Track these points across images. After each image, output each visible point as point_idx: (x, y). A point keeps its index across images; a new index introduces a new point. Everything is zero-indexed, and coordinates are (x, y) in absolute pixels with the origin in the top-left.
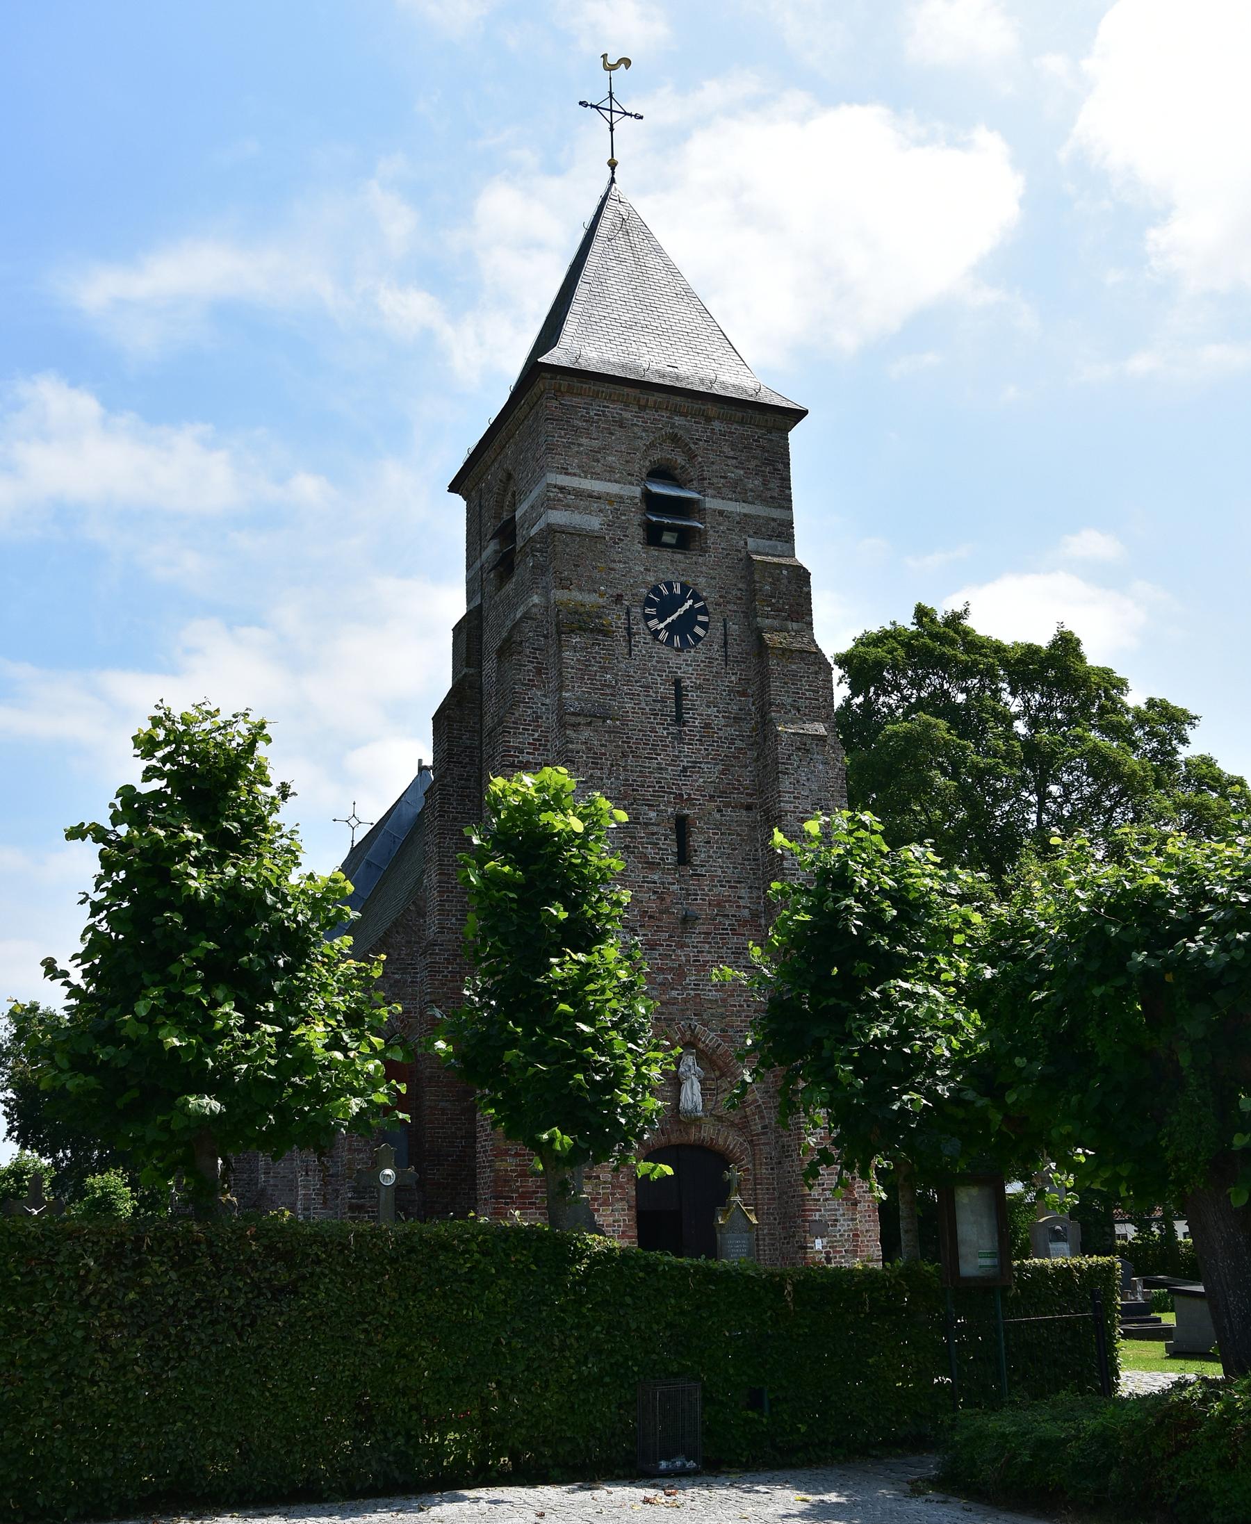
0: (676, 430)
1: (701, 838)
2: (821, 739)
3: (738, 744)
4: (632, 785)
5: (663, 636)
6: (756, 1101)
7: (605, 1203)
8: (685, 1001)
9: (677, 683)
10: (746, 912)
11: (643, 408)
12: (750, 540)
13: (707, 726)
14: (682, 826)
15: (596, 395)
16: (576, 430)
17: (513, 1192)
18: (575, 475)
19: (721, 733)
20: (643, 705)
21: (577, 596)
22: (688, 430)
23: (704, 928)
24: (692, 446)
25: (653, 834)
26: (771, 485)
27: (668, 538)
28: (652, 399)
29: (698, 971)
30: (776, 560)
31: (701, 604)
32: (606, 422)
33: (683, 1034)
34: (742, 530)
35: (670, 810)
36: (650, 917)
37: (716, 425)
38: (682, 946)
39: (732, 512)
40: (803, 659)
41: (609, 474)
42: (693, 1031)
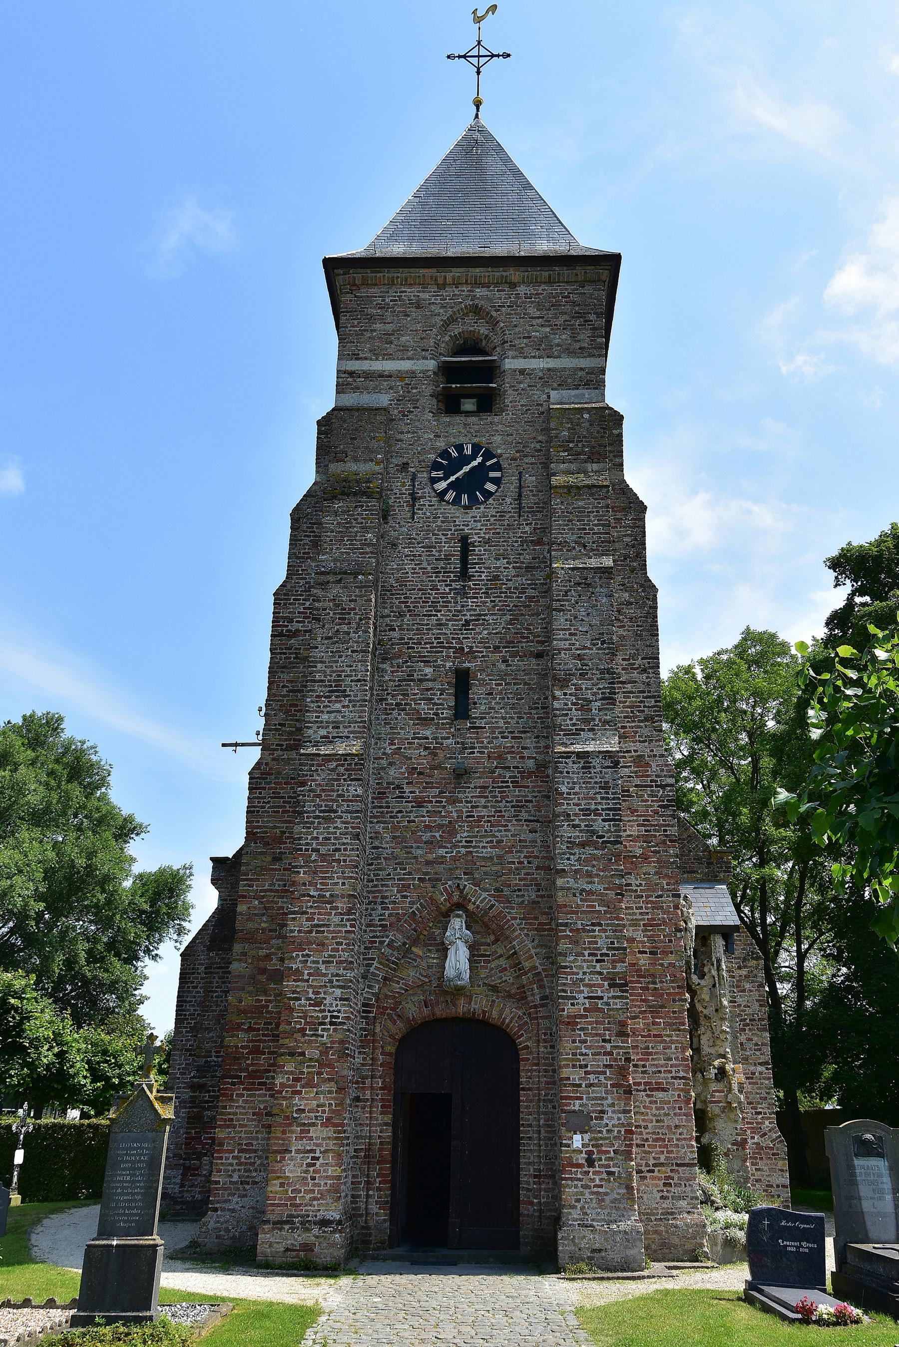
0: (476, 302)
1: (483, 690)
2: (605, 572)
3: (530, 592)
4: (406, 643)
5: (450, 496)
6: (536, 968)
7: (309, 1084)
8: (454, 859)
9: (464, 542)
10: (531, 763)
11: (443, 286)
12: (553, 394)
13: (496, 578)
14: (462, 681)
15: (392, 283)
16: (371, 318)
17: (241, 1070)
18: (366, 359)
19: (510, 584)
20: (425, 565)
21: (352, 466)
22: (489, 300)
23: (480, 782)
24: (494, 314)
25: (428, 690)
26: (581, 337)
27: (469, 405)
28: (449, 276)
29: (472, 827)
30: (567, 406)
31: (495, 460)
32: (401, 306)
33: (450, 895)
34: (546, 384)
35: (449, 664)
36: (420, 773)
37: (522, 290)
38: (454, 801)
39: (534, 369)
40: (592, 495)
41: (403, 353)
42: (462, 891)
